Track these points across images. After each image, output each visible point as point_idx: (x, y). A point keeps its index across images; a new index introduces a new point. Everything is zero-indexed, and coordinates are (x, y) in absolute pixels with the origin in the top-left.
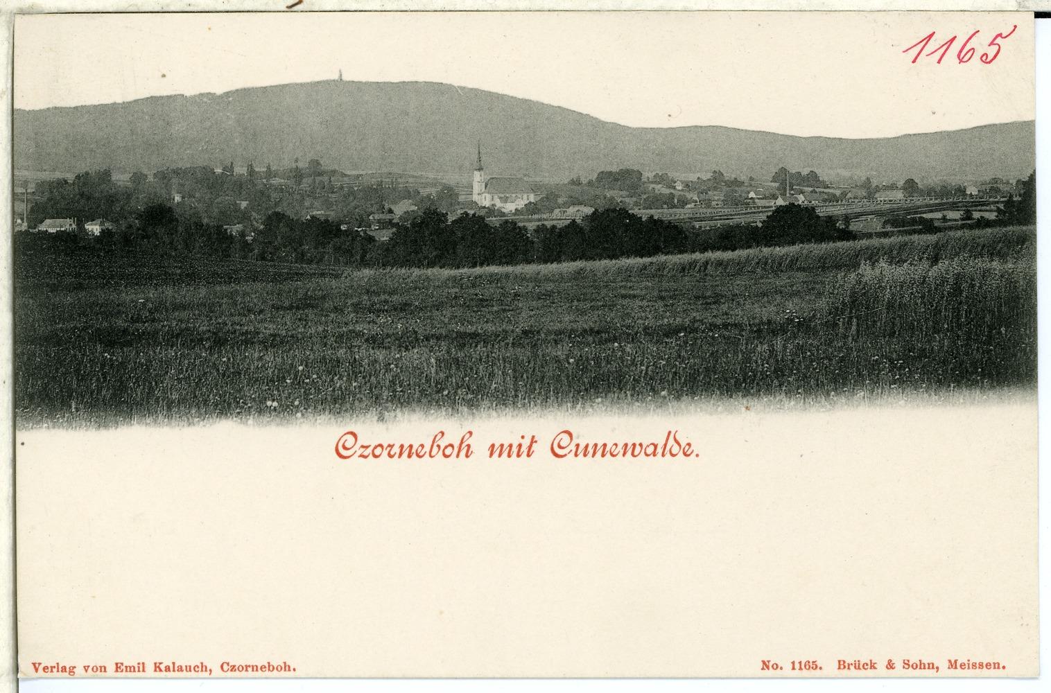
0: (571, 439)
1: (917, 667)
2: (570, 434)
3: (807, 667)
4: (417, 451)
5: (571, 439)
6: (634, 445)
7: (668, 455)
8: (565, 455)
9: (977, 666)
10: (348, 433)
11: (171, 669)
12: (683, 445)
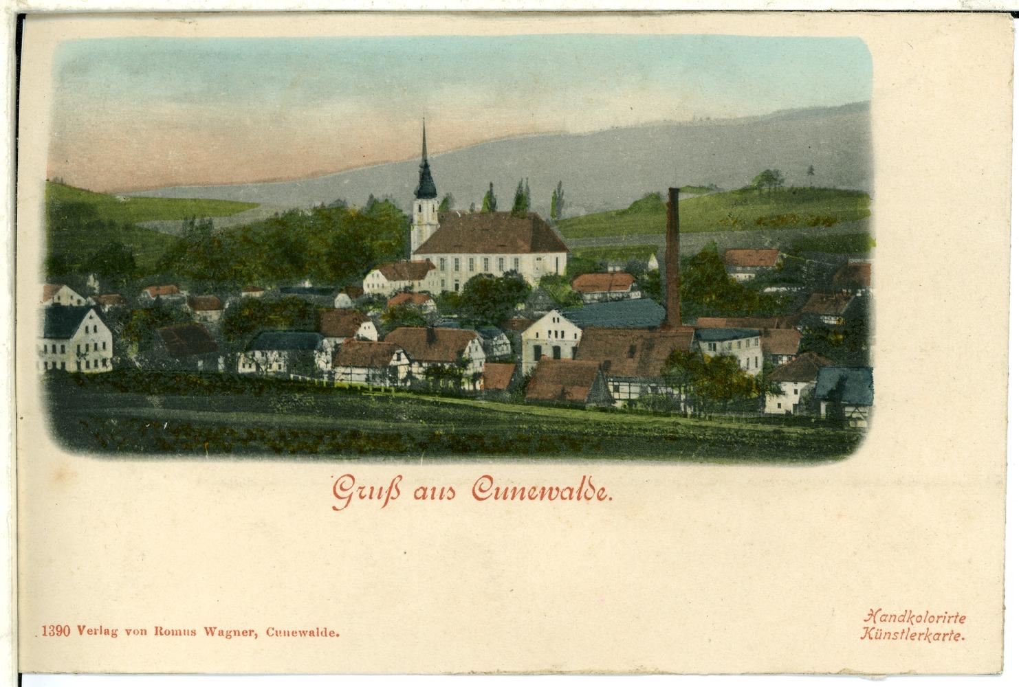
0: (492, 483)
1: (169, 633)
2: (491, 479)
3: (59, 629)
4: (529, 493)
5: (492, 483)
6: (551, 489)
7: (583, 498)
8: (482, 499)
9: (225, 633)
10: (483, 477)
11: (315, 634)
12: (597, 488)
